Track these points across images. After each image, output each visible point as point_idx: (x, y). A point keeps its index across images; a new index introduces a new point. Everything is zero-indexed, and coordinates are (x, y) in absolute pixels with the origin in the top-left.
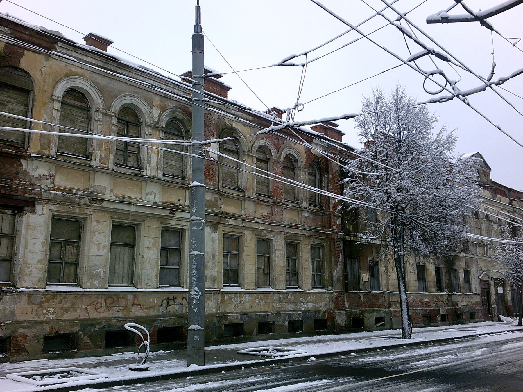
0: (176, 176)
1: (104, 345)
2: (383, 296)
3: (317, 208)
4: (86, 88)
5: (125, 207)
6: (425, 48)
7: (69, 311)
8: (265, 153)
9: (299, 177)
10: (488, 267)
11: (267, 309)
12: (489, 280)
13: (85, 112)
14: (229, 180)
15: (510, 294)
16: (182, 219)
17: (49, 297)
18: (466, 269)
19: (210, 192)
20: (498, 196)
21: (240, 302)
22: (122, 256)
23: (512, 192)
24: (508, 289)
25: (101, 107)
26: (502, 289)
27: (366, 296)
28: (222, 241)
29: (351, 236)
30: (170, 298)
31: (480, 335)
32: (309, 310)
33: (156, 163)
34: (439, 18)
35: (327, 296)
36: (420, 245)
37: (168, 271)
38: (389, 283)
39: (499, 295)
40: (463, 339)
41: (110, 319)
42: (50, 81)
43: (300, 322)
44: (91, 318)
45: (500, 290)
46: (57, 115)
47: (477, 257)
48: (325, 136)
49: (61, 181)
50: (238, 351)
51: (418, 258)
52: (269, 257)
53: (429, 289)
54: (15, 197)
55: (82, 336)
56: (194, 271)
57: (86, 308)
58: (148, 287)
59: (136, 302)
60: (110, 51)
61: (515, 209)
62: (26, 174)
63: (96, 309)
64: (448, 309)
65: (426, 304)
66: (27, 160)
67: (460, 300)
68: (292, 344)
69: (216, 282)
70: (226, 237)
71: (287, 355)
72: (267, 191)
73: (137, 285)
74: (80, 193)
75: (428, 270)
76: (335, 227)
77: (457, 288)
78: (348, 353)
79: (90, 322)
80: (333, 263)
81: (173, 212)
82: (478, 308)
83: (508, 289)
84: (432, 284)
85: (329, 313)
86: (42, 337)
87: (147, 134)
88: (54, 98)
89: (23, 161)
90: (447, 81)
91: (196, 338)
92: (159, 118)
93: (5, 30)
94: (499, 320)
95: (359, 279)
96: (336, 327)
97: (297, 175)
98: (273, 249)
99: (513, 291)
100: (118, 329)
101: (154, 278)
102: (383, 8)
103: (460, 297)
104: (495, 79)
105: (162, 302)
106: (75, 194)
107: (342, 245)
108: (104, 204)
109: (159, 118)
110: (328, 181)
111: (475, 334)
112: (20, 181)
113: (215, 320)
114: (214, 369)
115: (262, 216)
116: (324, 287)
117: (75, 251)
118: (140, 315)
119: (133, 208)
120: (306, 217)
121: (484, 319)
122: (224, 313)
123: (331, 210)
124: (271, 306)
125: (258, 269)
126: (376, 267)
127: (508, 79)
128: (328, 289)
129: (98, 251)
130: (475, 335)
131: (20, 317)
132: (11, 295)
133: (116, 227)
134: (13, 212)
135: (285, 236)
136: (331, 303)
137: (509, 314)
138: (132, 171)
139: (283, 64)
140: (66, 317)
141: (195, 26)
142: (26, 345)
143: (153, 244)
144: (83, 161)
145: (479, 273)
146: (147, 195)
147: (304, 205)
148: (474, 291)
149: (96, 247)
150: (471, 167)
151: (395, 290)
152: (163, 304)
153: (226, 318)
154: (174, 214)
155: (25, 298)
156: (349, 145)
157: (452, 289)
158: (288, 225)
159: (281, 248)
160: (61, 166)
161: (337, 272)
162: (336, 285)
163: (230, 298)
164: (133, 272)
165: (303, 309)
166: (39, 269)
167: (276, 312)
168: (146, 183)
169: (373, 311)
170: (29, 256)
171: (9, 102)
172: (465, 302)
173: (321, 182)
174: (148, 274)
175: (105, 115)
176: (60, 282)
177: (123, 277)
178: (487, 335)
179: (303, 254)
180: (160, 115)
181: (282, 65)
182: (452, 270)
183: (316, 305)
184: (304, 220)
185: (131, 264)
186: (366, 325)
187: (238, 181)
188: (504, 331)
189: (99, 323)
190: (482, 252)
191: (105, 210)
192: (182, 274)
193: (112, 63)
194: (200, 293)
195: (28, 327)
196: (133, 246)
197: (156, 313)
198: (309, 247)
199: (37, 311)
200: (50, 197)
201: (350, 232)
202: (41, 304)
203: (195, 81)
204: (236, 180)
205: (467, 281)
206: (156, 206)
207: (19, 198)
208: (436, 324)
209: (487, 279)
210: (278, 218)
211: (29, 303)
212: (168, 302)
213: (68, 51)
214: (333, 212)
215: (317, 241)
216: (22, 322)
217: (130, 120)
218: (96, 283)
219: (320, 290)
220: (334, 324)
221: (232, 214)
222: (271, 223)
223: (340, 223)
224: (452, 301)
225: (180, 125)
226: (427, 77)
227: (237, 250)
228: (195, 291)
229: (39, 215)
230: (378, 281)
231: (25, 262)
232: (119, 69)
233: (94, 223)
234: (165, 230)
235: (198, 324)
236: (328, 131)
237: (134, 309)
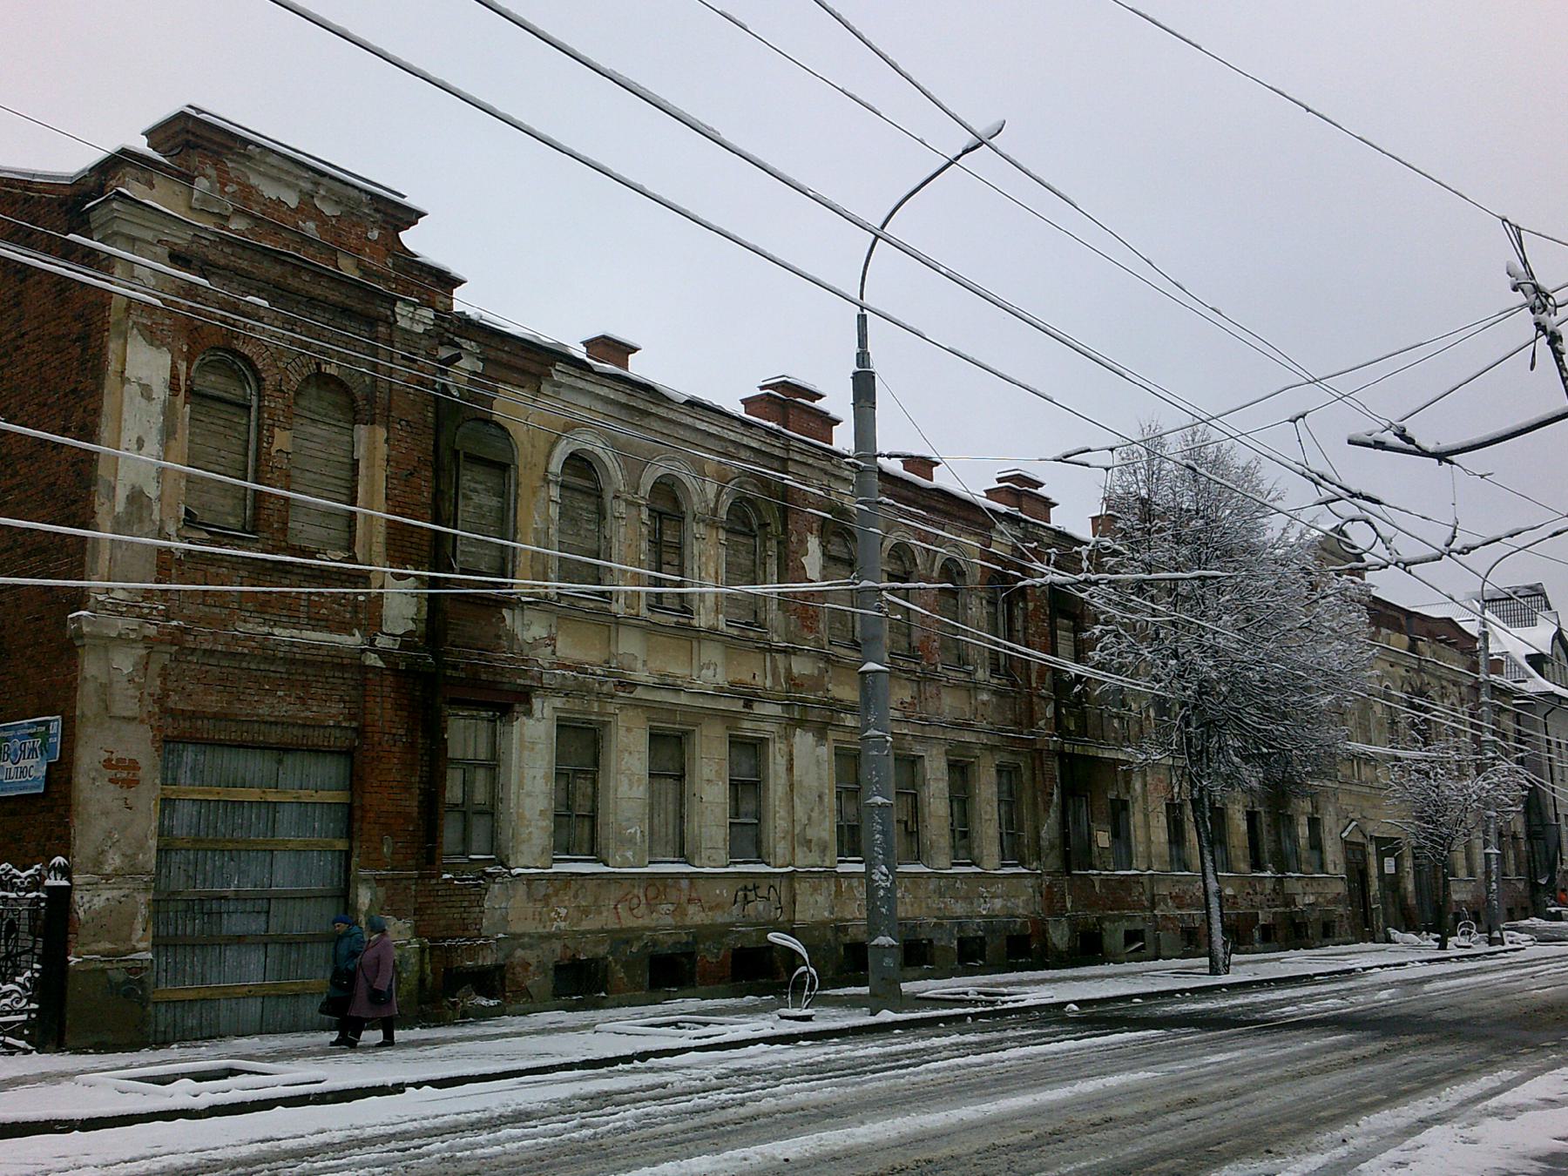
0: (746, 624)
1: (646, 984)
2: (1138, 882)
3: (1004, 681)
4: (598, 451)
5: (669, 697)
7: (590, 913)
8: (902, 561)
9: (969, 612)
10: (1363, 810)
11: (917, 912)
12: (1364, 841)
13: (593, 499)
14: (838, 625)
15: (1411, 876)
16: (763, 718)
17: (558, 887)
18: (1312, 814)
19: (810, 657)
20: (1384, 631)
22: (663, 800)
23: (1415, 621)
24: (1408, 863)
25: (622, 489)
26: (1393, 863)
27: (1105, 882)
29: (1075, 743)
30: (749, 886)
31: (1364, 969)
32: (997, 916)
33: (713, 599)
34: (1370, 440)
35: (1028, 882)
38: (1150, 852)
40: (1332, 976)
41: (654, 929)
42: (542, 446)
43: (978, 941)
44: (1430, 941)
46: (554, 511)
47: (1336, 785)
48: (1020, 514)
49: (567, 649)
50: (919, 995)
52: (916, 795)
53: (1234, 864)
54: (499, 686)
55: (613, 964)
56: (877, 836)
57: (616, 908)
58: (712, 864)
59: (694, 895)
60: (638, 368)
61: (1423, 663)
62: (513, 637)
64: (1275, 913)
65: (1228, 900)
66: (513, 610)
67: (1300, 890)
68: (1020, 983)
70: (839, 753)
71: (1023, 1001)
72: (907, 646)
73: (693, 858)
74: (599, 672)
75: (1231, 819)
76: (1041, 723)
77: (1293, 862)
78: (1127, 998)
80: (1041, 806)
81: (748, 704)
82: (1340, 910)
84: (1239, 853)
85: (1034, 922)
86: (551, 966)
87: (697, 538)
88: (550, 477)
89: (505, 612)
90: (1378, 535)
91: (888, 962)
92: (717, 501)
93: (472, 347)
95: (1090, 840)
96: (1049, 953)
97: (965, 606)
98: (924, 777)
99: (1417, 869)
100: (977, 931)
101: (721, 845)
102: (1480, 573)
103: (1300, 883)
104: (1456, 545)
105: (736, 895)
106: (591, 674)
107: (1056, 765)
108: (639, 693)
109: (717, 501)
110: (1026, 617)
111: (1352, 967)
112: (504, 652)
113: (830, 935)
114: (922, 1019)
115: (902, 703)
116: (1022, 864)
117: (589, 790)
118: (700, 922)
119: (683, 699)
120: (984, 704)
121: (1353, 938)
122: (841, 920)
123: (1034, 685)
124: (924, 905)
126: (1123, 815)
127: (1477, 547)
128: (1032, 867)
130: (1353, 970)
131: (516, 928)
132: (502, 883)
133: (656, 738)
134: (494, 715)
135: (947, 747)
136: (1038, 898)
137: (1409, 925)
138: (675, 619)
139: (1064, 459)
140: (585, 925)
141: (858, 354)
142: (528, 983)
143: (716, 771)
144: (599, 605)
145: (1341, 825)
146: (701, 668)
147: (982, 675)
148: (1331, 868)
149: (627, 781)
150: (1353, 601)
151: (1165, 868)
152: (738, 899)
153: (845, 928)
154: (751, 707)
155: (522, 888)
156: (1067, 531)
157: (1282, 865)
158: (952, 723)
159: (939, 775)
160: (566, 618)
161: (1049, 829)
162: (1047, 855)
163: (850, 887)
164: (682, 833)
165: (984, 913)
166: (542, 828)
167: (935, 920)
168: (699, 642)
169: (1121, 917)
170: (527, 802)
171: (475, 490)
172: (1311, 897)
173: (1010, 619)
175: (629, 503)
176: (568, 854)
177: (667, 843)
178: (1379, 970)
179: (982, 787)
180: (718, 495)
181: (1061, 460)
182: (1283, 821)
183: (1009, 904)
184: (981, 708)
185: (678, 816)
187: (853, 627)
188: (1413, 962)
189: (639, 938)
190: (1349, 772)
191: (638, 704)
192: (764, 837)
193: (643, 395)
194: (891, 877)
195: (531, 947)
196: (680, 778)
197: (726, 919)
198: (993, 771)
199: (540, 913)
200: (555, 683)
201: (1070, 733)
202: (547, 897)
203: (863, 464)
204: (850, 625)
205: (1316, 844)
206: (719, 692)
207: (506, 687)
208: (1250, 947)
209: (1360, 840)
210: (931, 707)
211: (528, 898)
212: (746, 896)
214: (1037, 689)
215: (1007, 758)
216: (522, 935)
217: (665, 509)
218: (629, 854)
219: (1015, 870)
220: (1046, 945)
221: (848, 703)
222: (921, 719)
223: (1052, 715)
224: (1284, 894)
225: (749, 510)
226: (1485, 581)
227: (857, 782)
228: (882, 873)
229: (538, 720)
230: (1129, 846)
231: (520, 817)
232: (652, 406)
233: (622, 732)
234: (737, 743)
235: (890, 936)
236: (1024, 499)
237: (692, 909)
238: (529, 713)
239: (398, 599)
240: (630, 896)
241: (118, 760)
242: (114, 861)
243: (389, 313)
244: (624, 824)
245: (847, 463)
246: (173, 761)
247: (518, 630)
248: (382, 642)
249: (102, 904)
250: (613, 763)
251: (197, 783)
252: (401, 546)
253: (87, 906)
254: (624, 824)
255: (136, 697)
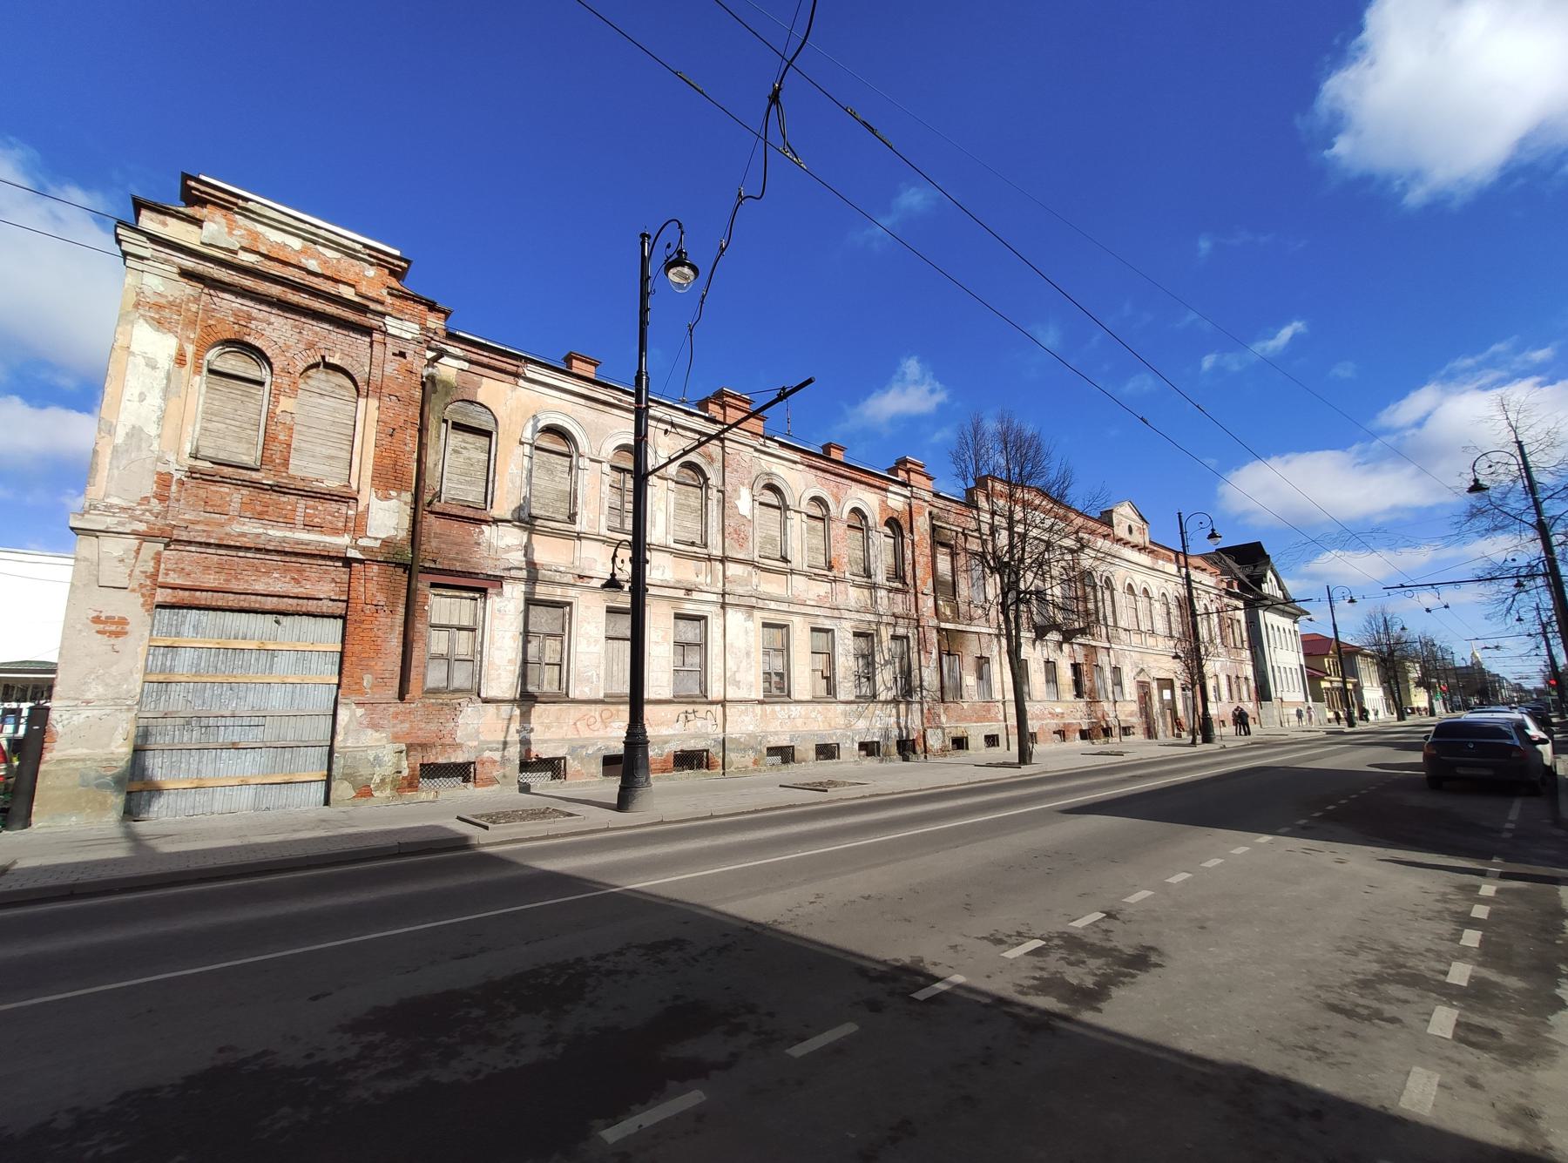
6: (746, 412)
21: (789, 717)
24: (1178, 692)
28: (646, 373)
36: (1304, 550)
37: (686, 673)
39: (1165, 702)
45: (1167, 694)
51: (1045, 652)
57: (575, 724)
63: (588, 725)
69: (753, 689)
79: (581, 743)
83: (1178, 692)
84: (1067, 687)
94: (782, 557)
115: (818, 596)
125: (813, 670)
129: (588, 647)
149: (585, 641)
166: (510, 671)
171: (465, 448)
174: (657, 679)
186: (932, 746)
213: (77, 763)
227: (349, 482)
238: (500, 594)
239: (381, 513)
240: (588, 717)
241: (107, 618)
242: (95, 690)
243: (382, 324)
244: (582, 669)
245: (1021, 937)
246: (177, 620)
247: (494, 541)
248: (363, 542)
249: (81, 720)
250: (518, 669)
251: (199, 636)
252: (387, 479)
253: (66, 722)
254: (582, 669)
255: (125, 574)
